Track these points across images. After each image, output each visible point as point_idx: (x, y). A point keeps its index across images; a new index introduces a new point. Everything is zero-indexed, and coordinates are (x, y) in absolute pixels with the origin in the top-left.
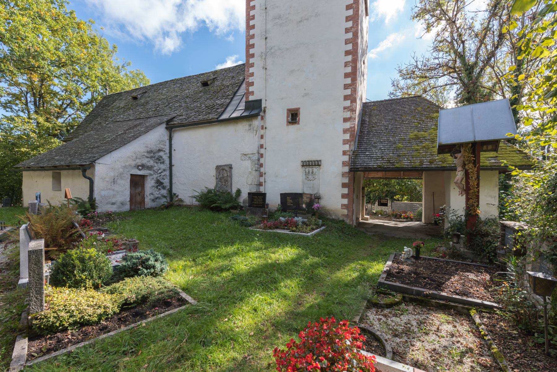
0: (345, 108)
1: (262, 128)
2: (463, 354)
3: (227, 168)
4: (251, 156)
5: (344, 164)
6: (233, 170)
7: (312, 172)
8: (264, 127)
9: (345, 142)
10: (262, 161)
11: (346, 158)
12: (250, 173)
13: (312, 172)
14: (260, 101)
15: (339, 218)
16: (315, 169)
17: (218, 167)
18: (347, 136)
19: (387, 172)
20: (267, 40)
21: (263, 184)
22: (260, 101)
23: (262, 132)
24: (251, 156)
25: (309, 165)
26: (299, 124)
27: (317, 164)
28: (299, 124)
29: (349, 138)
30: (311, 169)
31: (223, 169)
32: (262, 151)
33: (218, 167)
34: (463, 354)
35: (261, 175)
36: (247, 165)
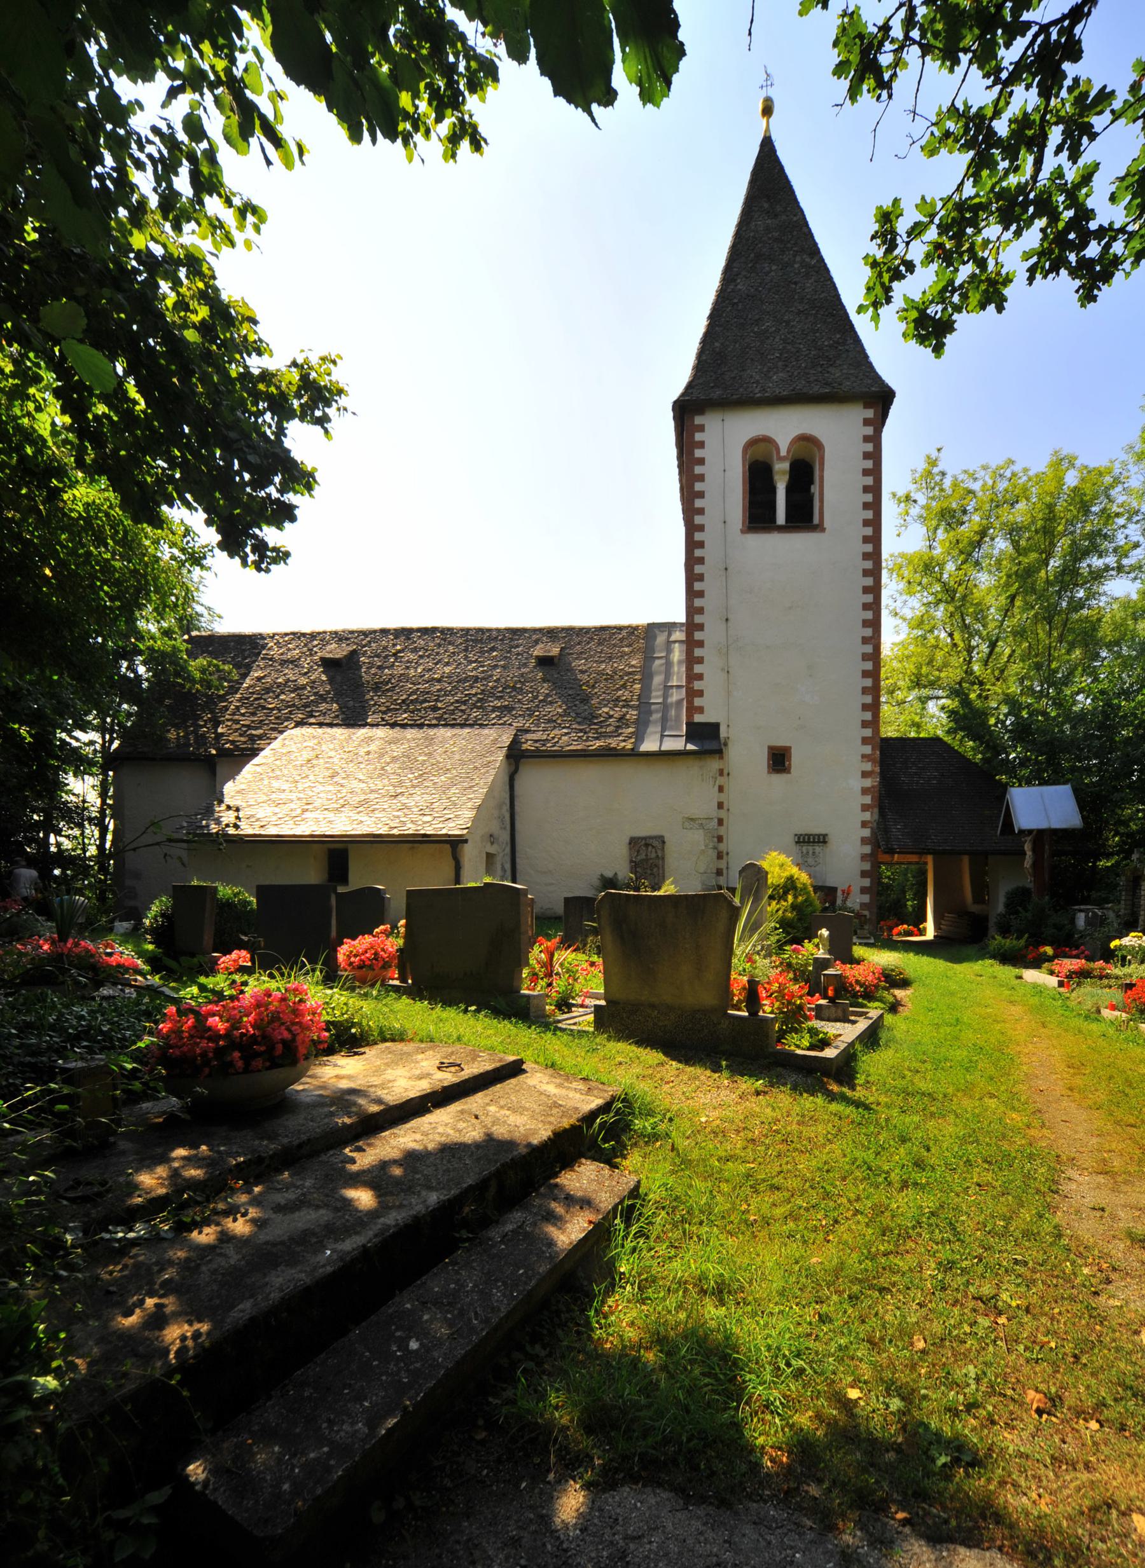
0: (863, 756)
1: (721, 773)
2: (1095, 1317)
3: (655, 843)
4: (704, 822)
5: (864, 841)
6: (667, 846)
7: (814, 853)
8: (725, 772)
9: (865, 808)
10: (722, 831)
11: (867, 833)
12: (703, 852)
13: (814, 853)
14: (715, 727)
15: (426, 1148)
16: (818, 849)
17: (634, 842)
18: (868, 800)
19: (684, 647)
20: (730, 624)
21: (725, 872)
22: (715, 727)
23: (721, 781)
24: (704, 822)
25: (809, 842)
26: (789, 772)
27: (821, 840)
28: (789, 772)
29: (869, 802)
30: (810, 848)
31: (647, 845)
32: (722, 814)
33: (634, 842)
34: (1095, 1317)
35: (720, 856)
36: (697, 838)
